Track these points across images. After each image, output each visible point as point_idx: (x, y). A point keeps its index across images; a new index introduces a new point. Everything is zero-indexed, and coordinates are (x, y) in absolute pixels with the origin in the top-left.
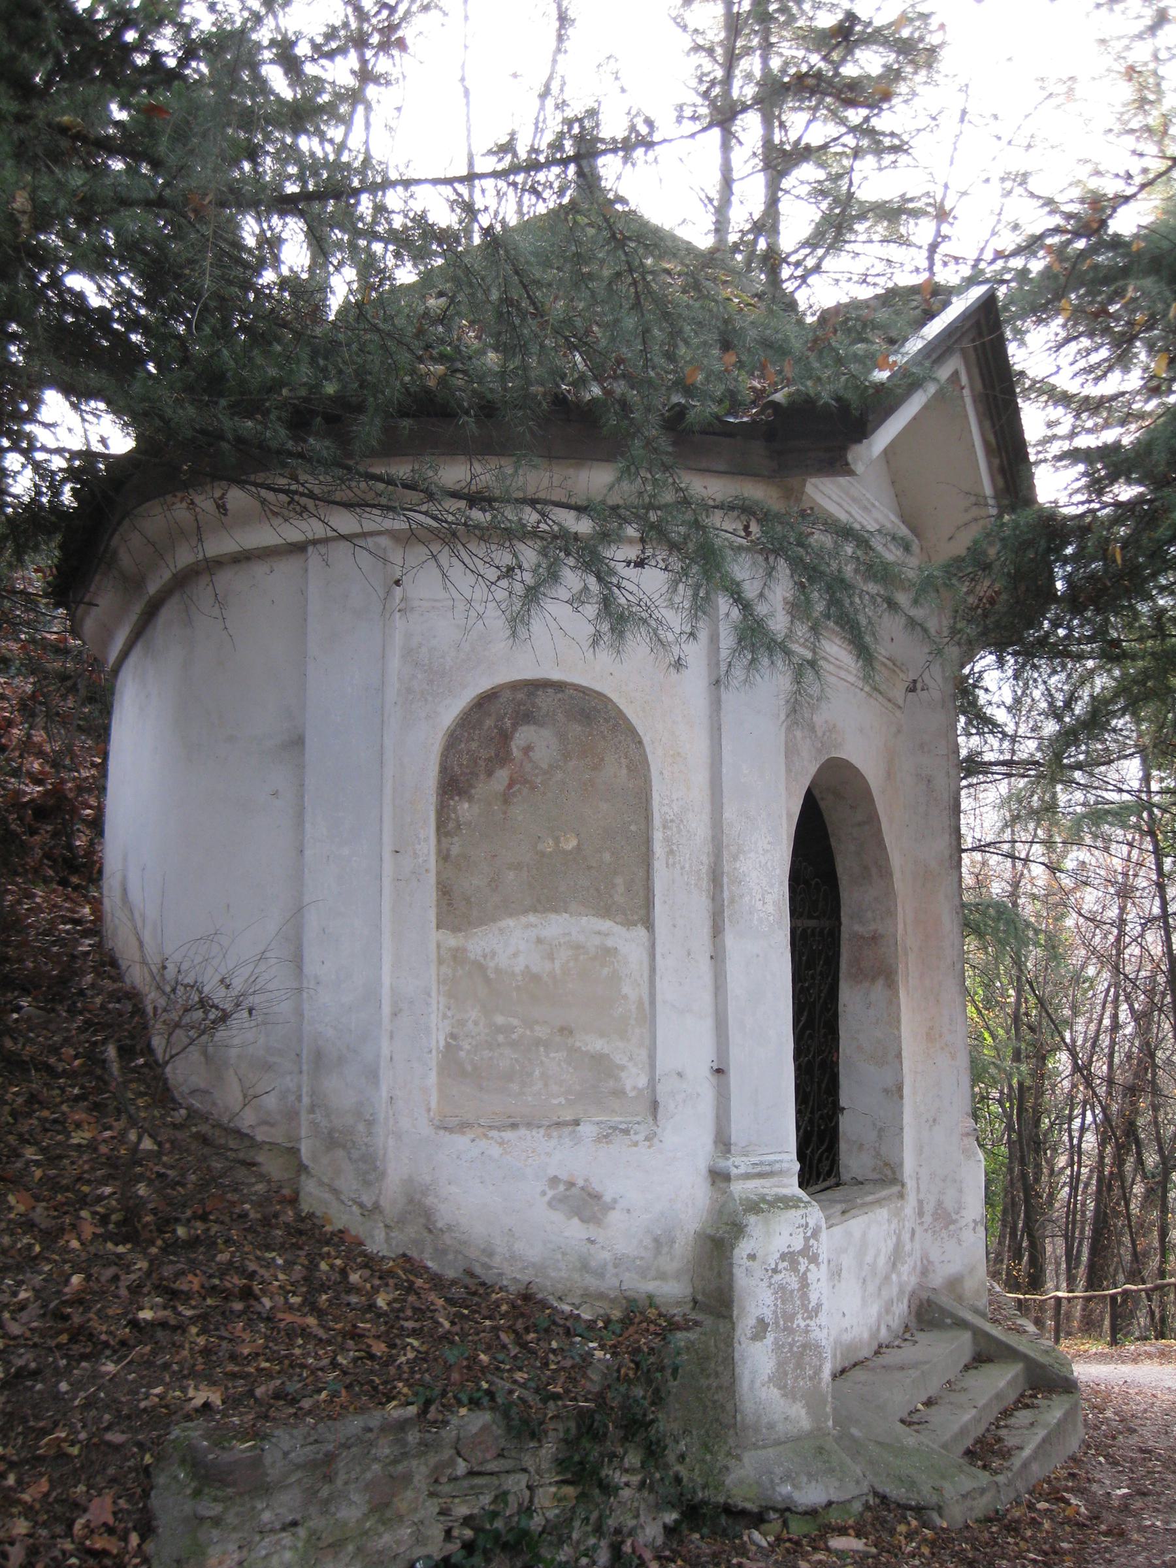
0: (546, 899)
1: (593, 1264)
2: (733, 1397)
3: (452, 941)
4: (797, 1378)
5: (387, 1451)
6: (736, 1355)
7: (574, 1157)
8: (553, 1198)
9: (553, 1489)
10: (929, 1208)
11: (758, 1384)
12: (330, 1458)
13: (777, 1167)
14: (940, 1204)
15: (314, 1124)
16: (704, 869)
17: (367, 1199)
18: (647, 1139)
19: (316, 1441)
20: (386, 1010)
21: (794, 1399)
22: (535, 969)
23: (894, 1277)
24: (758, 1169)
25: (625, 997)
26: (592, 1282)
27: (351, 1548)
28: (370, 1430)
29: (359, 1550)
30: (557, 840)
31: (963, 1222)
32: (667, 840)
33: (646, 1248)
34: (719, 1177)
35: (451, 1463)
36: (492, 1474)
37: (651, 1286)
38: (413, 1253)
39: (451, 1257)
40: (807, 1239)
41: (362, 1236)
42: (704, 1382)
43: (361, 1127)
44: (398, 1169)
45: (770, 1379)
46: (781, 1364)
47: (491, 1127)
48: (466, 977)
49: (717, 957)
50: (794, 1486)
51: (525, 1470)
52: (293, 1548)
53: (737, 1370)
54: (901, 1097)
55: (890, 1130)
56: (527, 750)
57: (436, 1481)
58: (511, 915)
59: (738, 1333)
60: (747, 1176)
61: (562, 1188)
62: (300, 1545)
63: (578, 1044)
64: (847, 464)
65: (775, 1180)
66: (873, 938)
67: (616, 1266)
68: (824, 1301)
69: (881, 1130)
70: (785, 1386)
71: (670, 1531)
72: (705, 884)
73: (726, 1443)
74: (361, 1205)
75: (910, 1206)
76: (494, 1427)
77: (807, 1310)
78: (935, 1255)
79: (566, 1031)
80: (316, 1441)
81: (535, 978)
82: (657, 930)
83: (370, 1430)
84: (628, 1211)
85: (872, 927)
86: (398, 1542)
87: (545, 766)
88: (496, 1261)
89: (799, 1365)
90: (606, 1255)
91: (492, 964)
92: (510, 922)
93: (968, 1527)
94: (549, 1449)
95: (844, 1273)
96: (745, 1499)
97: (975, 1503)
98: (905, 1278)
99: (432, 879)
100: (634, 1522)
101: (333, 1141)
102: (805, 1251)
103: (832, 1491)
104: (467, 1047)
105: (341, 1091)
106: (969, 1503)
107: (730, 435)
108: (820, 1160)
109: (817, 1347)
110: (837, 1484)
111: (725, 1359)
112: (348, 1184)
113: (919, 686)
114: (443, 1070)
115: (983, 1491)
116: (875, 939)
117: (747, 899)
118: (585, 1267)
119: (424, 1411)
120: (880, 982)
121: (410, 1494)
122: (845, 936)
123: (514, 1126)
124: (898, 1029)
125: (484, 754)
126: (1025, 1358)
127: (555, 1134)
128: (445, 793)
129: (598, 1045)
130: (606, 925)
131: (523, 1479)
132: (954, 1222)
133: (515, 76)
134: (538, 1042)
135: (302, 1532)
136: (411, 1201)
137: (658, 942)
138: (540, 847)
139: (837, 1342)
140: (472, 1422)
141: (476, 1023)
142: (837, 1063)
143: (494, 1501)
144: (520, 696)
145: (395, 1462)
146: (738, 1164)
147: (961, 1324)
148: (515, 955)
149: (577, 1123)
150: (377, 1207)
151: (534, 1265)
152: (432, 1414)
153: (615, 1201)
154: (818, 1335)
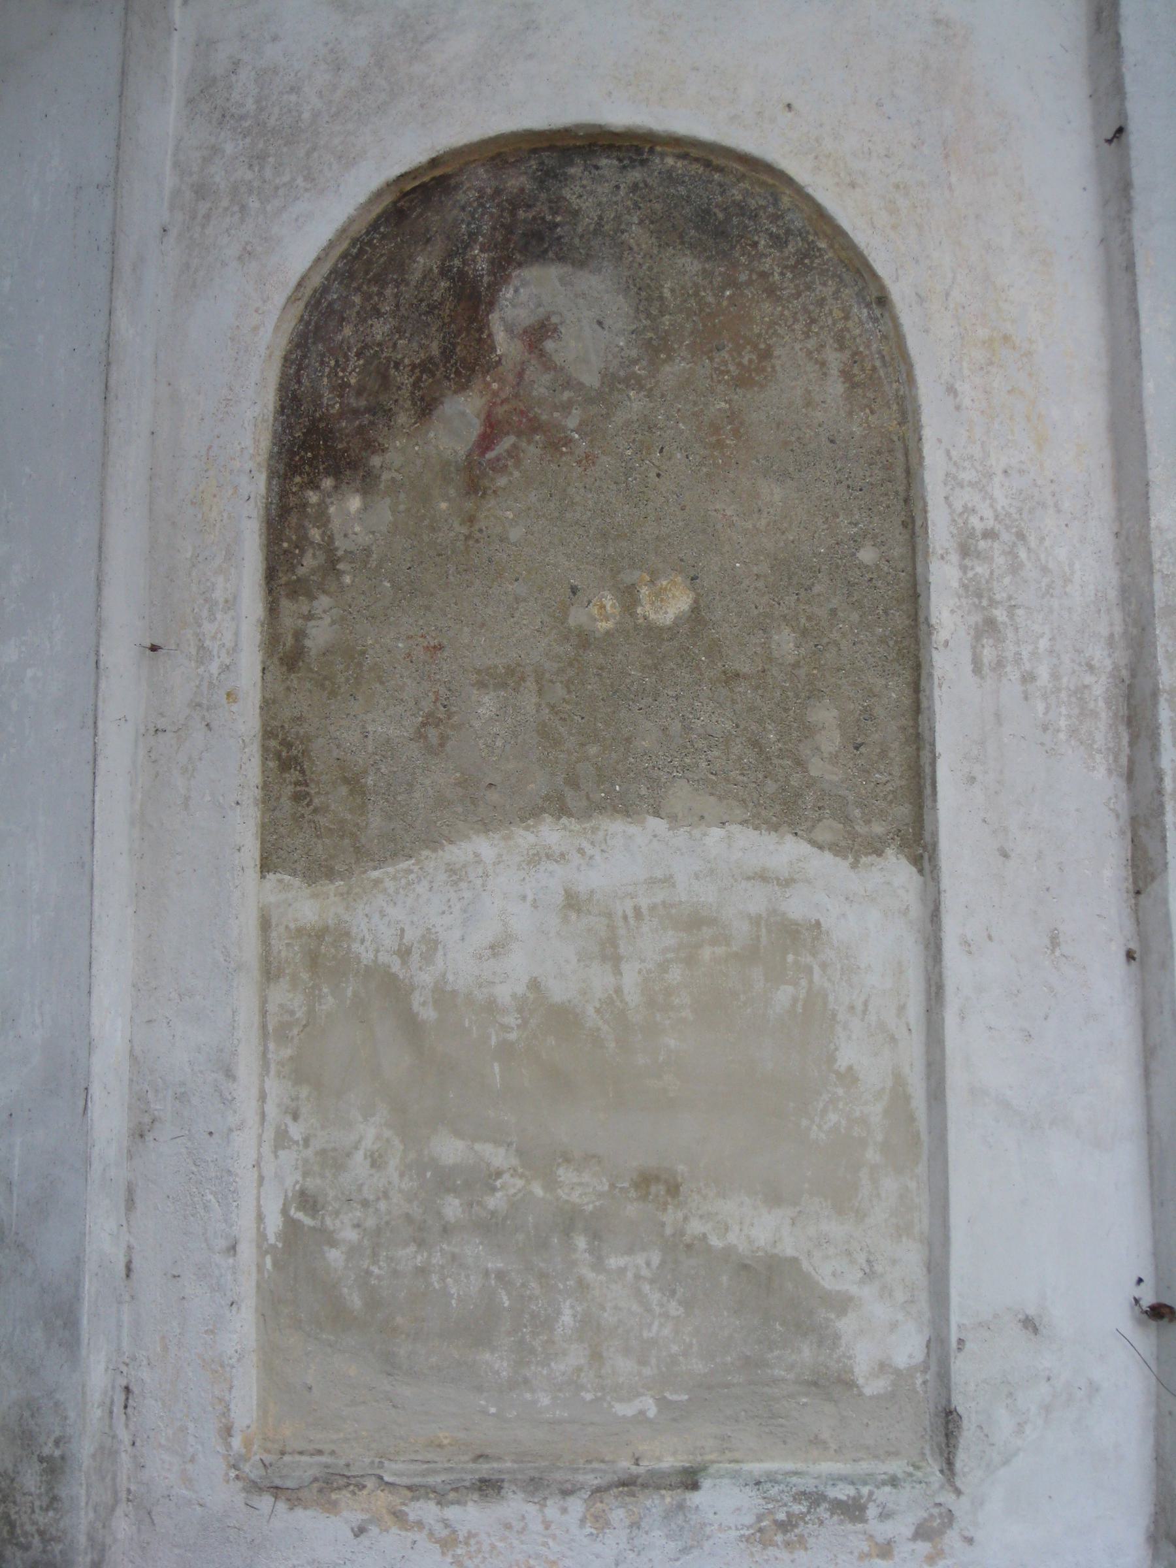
0: (594, 779)
3: (306, 906)
16: (1099, 687)
18: (923, 1532)
20: (109, 1120)
22: (559, 992)
25: (850, 1077)
30: (629, 597)
32: (976, 593)
43: (31, 1479)
48: (345, 1016)
56: (538, 335)
58: (485, 827)
63: (696, 1227)
79: (658, 1184)
81: (563, 1019)
87: (591, 379)
91: (426, 978)
92: (485, 847)
99: (246, 719)
104: (351, 1235)
114: (273, 1305)
123: (488, 1487)
125: (408, 350)
127: (618, 1515)
128: (293, 469)
129: (757, 1228)
130: (785, 851)
134: (569, 1220)
138: (577, 617)
141: (376, 1162)
144: (517, 181)
148: (497, 949)
149: (690, 1480)
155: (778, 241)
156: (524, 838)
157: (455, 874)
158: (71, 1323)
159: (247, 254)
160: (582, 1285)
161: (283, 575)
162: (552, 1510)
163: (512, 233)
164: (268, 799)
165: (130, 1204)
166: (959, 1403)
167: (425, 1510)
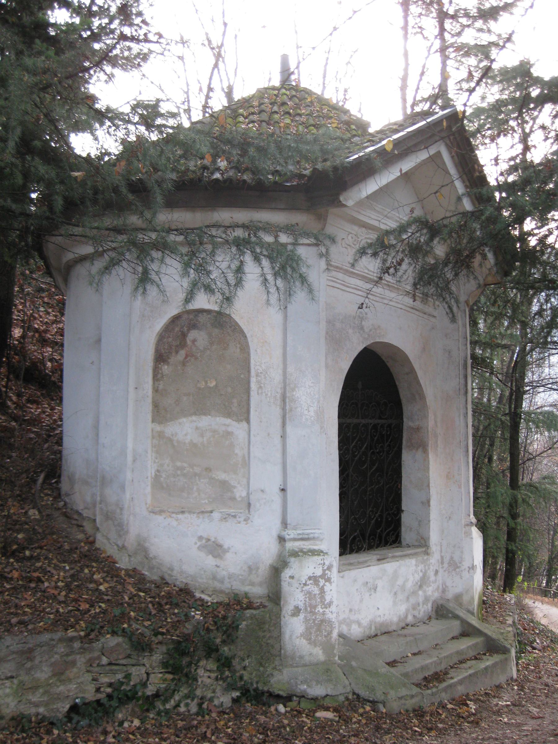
0: (200, 409)
1: (218, 577)
2: (280, 642)
3: (158, 428)
4: (317, 636)
5: (63, 650)
6: (282, 623)
7: (210, 527)
8: (200, 546)
9: (161, 675)
10: (446, 560)
11: (294, 637)
12: (31, 650)
13: (311, 536)
14: (452, 558)
15: (101, 509)
16: (279, 396)
17: (120, 543)
18: (245, 520)
19: (25, 643)
20: (130, 458)
21: (315, 646)
22: (195, 442)
23: (420, 593)
24: (300, 537)
25: (237, 454)
26: (218, 585)
27: (41, 691)
28: (53, 640)
29: (46, 692)
30: (206, 382)
31: (463, 568)
32: (258, 382)
33: (244, 571)
34: (282, 540)
35: (99, 658)
36: (124, 665)
37: (247, 589)
38: (139, 568)
39: (155, 570)
40: (324, 571)
41: (117, 559)
42: (261, 634)
43: (118, 511)
44: (135, 529)
45: (301, 635)
46: (307, 629)
47: (173, 513)
48: (164, 444)
49: (283, 437)
50: (308, 686)
51: (144, 665)
52: (11, 687)
53: (282, 630)
54: (429, 506)
55: (424, 522)
56: (194, 341)
57: (91, 666)
58: (185, 416)
59: (284, 612)
60: (295, 540)
61: (204, 541)
62: (15, 686)
63: (214, 476)
64: (340, 202)
65: (311, 542)
66: (418, 429)
67: (229, 578)
68: (334, 600)
69: (420, 521)
70: (310, 639)
71: (235, 701)
72: (279, 402)
73: (273, 663)
74: (118, 546)
75: (434, 559)
76: (124, 644)
77: (324, 604)
78: (449, 583)
79: (208, 469)
80: (25, 643)
81: (195, 445)
82: (251, 423)
83: (53, 640)
84: (236, 553)
85: (417, 423)
86: (69, 691)
87: (201, 348)
88: (175, 573)
89: (319, 629)
90: (224, 573)
91: (175, 439)
92: (184, 420)
93: (400, 713)
94: (157, 657)
95: (378, 589)
96: (280, 690)
97: (407, 702)
98: (430, 593)
99: (150, 400)
100: (213, 695)
101: (108, 517)
102: (323, 576)
103: (329, 690)
104: (164, 476)
105: (111, 495)
106: (403, 701)
107: (286, 191)
108: (388, 534)
109: (330, 622)
110: (332, 687)
111: (275, 624)
112: (113, 535)
113: (364, 306)
114: (153, 486)
115: (412, 697)
116: (418, 429)
117: (299, 409)
118: (214, 578)
119: (87, 635)
120: (420, 450)
121: (75, 670)
122: (405, 427)
123: (183, 512)
124: (428, 473)
125: (174, 343)
126: (485, 635)
127: (201, 516)
128: (157, 361)
129: (222, 476)
130: (228, 421)
131: (143, 670)
132: (458, 567)
133: (264, 27)
134: (195, 475)
135: (15, 681)
136: (139, 544)
137: (252, 429)
138: (199, 385)
139: (371, 622)
140: (111, 641)
141: (168, 466)
142: (400, 489)
143: (124, 678)
144: (191, 317)
145: (67, 655)
146: (290, 534)
147: (456, 617)
148: (186, 435)
149: (211, 512)
150: (124, 547)
151: (191, 576)
152: (92, 636)
153: (229, 548)
154: (329, 616)
155: (230, 327)
156: (190, 418)
157: (180, 423)
158: (124, 488)
159: (150, 327)
160: (197, 484)
161: (155, 378)
162: (192, 515)
163: (268, 124)
164: (153, 412)
165: (133, 471)
166: (251, 502)
167: (174, 515)
